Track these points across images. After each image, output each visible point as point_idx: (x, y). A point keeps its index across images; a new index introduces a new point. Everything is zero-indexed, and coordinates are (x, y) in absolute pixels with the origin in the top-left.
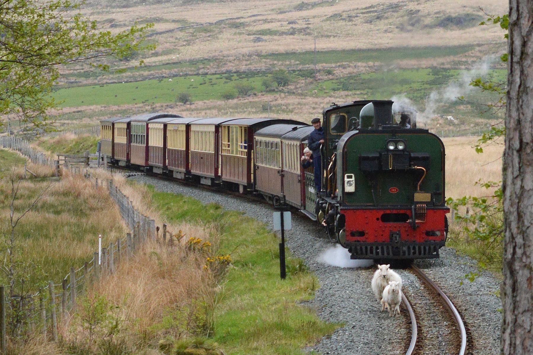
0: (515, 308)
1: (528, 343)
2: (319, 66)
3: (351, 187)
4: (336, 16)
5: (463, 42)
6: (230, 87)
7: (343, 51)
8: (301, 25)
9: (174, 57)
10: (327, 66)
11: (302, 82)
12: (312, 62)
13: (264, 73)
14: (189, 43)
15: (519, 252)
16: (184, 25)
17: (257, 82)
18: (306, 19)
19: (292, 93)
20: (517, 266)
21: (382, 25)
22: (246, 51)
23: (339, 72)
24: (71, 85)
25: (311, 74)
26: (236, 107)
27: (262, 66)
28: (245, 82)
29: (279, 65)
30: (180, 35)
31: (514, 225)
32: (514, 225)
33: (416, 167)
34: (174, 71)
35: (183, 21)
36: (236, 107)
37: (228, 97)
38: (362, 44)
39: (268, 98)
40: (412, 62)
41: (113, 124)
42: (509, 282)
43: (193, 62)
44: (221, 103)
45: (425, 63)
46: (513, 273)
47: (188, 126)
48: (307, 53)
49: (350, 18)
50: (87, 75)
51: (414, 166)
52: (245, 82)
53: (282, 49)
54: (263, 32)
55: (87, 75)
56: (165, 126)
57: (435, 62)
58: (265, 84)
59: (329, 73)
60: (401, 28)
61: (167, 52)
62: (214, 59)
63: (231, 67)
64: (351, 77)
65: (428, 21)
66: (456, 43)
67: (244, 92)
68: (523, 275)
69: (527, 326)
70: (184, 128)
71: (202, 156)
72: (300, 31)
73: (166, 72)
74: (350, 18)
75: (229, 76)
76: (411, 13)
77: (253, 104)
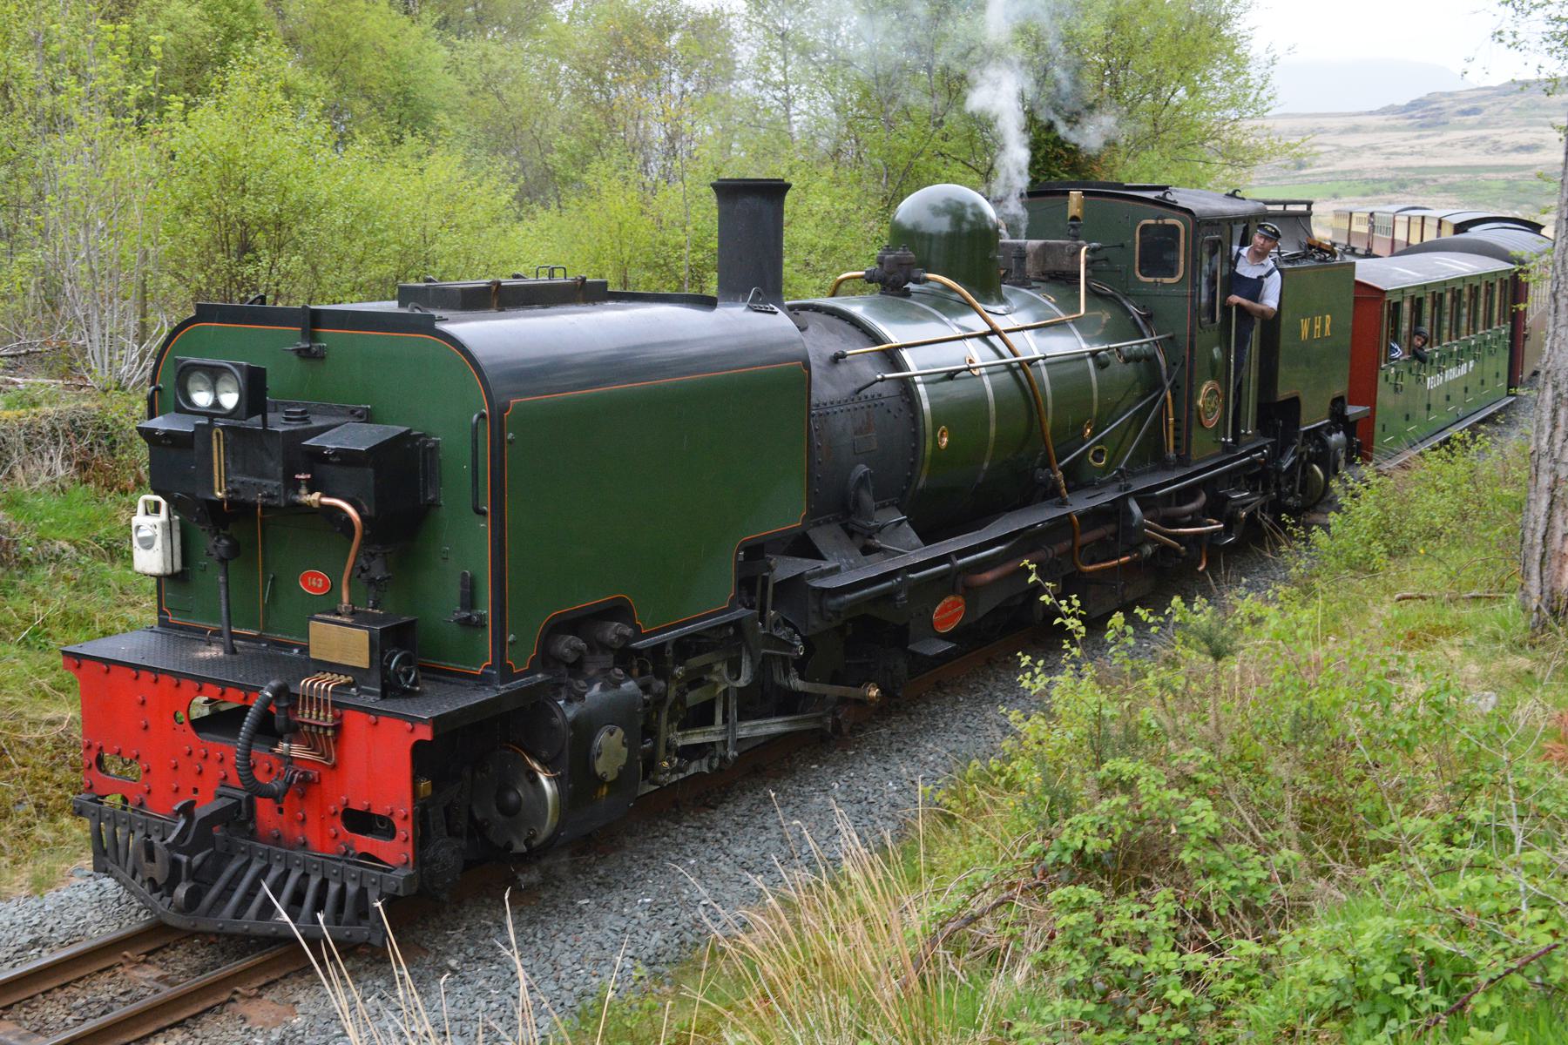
0: (1556, 323)
1: (1563, 347)
2: (1428, 176)
3: (150, 551)
4: (1443, 144)
5: (1530, 163)
6: (1367, 188)
7: (1446, 167)
8: (1418, 149)
9: (1330, 169)
10: (1434, 176)
11: (1416, 186)
12: (1424, 173)
13: (1390, 180)
14: (1341, 159)
15: (1561, 286)
16: (1339, 148)
17: (1385, 186)
18: (1422, 145)
19: (1408, 193)
20: (1559, 296)
21: (1474, 150)
22: (1379, 165)
23: (1442, 181)
24: (1261, 185)
25: (1422, 181)
26: (1370, 201)
27: (1389, 175)
28: (1377, 186)
29: (1401, 175)
30: (1336, 154)
31: (1559, 269)
32: (1559, 269)
33: (316, 495)
34: (1331, 177)
35: (1338, 145)
36: (1370, 201)
37: (1365, 195)
38: (1459, 162)
39: (1392, 197)
40: (1493, 175)
41: (1351, 214)
42: (1553, 306)
43: (1343, 172)
44: (1359, 199)
45: (1502, 176)
46: (1556, 300)
47: (1423, 218)
48: (1420, 167)
49: (1452, 145)
50: (1272, 179)
51: (311, 492)
52: (1377, 186)
53: (1404, 164)
54: (1392, 154)
55: (1272, 179)
56: (1423, 218)
57: (1510, 176)
58: (1391, 188)
59: (1435, 181)
60: (1487, 152)
61: (1326, 165)
62: (1358, 170)
63: (1368, 175)
64: (1450, 184)
65: (1505, 148)
66: (1523, 163)
67: (1376, 192)
68: (1562, 302)
69: (1563, 336)
70: (1420, 221)
71: (1359, 235)
72: (1417, 153)
73: (1325, 178)
74: (1452, 145)
75: (1366, 181)
76: (1496, 142)
77: (1381, 201)
